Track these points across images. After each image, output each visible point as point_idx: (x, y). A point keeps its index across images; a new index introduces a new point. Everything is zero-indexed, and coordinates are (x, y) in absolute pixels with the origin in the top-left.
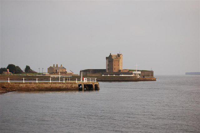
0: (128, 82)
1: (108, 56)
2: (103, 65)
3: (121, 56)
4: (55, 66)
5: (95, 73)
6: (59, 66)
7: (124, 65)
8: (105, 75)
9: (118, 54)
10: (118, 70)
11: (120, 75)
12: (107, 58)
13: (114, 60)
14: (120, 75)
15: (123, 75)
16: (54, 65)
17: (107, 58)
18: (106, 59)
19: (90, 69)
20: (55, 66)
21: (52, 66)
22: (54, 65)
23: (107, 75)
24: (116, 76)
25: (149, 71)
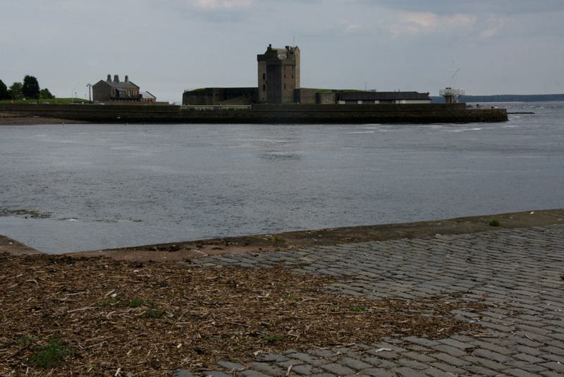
0: (419, 127)
1: (263, 51)
2: (249, 78)
3: (296, 53)
4: (113, 79)
5: (226, 99)
6: (122, 79)
7: (316, 74)
8: (366, 103)
9: (287, 47)
10: (292, 90)
11: (397, 102)
12: (260, 58)
13: (283, 63)
14: (397, 102)
15: (404, 102)
16: (109, 76)
17: (260, 58)
18: (258, 60)
19: (212, 89)
20: (113, 79)
21: (105, 79)
22: (109, 76)
23: (371, 103)
24: (348, 106)
25: (68, 259)
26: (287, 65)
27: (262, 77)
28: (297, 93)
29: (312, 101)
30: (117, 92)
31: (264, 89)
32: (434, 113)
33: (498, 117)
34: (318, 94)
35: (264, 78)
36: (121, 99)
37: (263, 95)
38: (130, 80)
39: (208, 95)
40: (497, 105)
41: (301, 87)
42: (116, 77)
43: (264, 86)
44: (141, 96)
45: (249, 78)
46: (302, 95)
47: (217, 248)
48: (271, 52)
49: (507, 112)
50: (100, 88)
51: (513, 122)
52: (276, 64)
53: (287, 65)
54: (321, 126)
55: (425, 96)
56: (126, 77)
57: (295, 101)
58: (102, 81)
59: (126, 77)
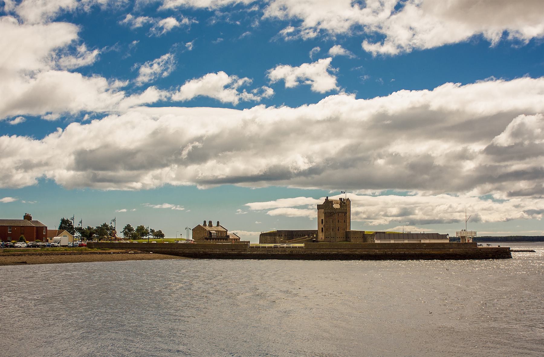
4: (207, 224)
16: (205, 222)
20: (207, 224)
22: (205, 222)
26: (340, 213)
28: (348, 235)
29: (360, 241)
30: (211, 233)
31: (322, 231)
32: (451, 250)
33: (505, 254)
34: (363, 236)
35: (322, 222)
36: (213, 239)
37: (321, 236)
39: (279, 236)
40: (503, 245)
41: (352, 229)
43: (322, 229)
44: (228, 236)
46: (352, 236)
47: (103, 253)
49: (511, 249)
50: (197, 230)
53: (340, 213)
54: (301, 261)
57: (346, 241)
58: (431, 89)
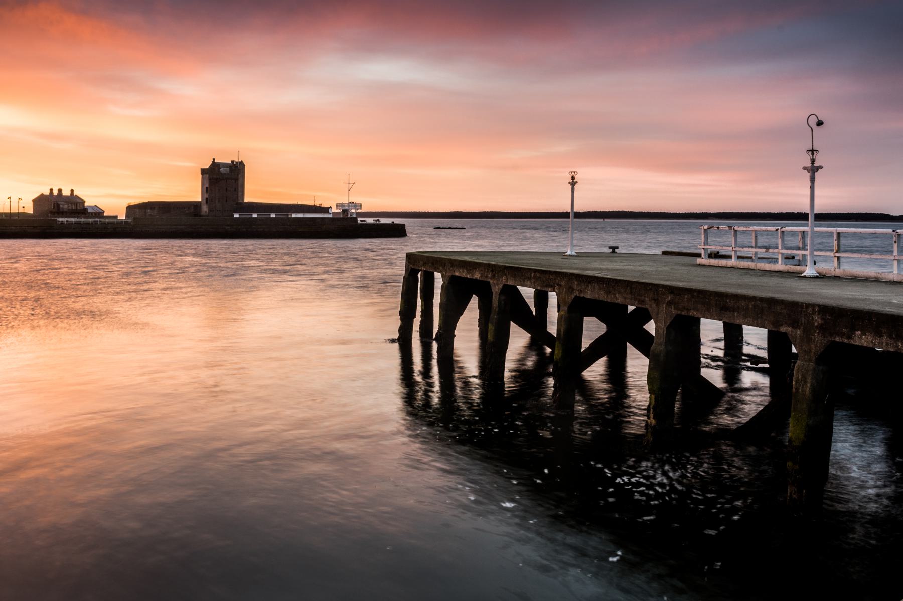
2: (189, 190)
6: (55, 193)
9: (233, 162)
12: (203, 172)
16: (51, 190)
17: (203, 172)
21: (47, 193)
22: (51, 190)
27: (206, 190)
37: (205, 208)
38: (75, 193)
42: (60, 191)
45: (189, 190)
48: (215, 166)
50: (39, 201)
51: (658, 251)
52: (224, 178)
55: (326, 210)
56: (72, 191)
58: (34, 201)
59: (72, 191)
